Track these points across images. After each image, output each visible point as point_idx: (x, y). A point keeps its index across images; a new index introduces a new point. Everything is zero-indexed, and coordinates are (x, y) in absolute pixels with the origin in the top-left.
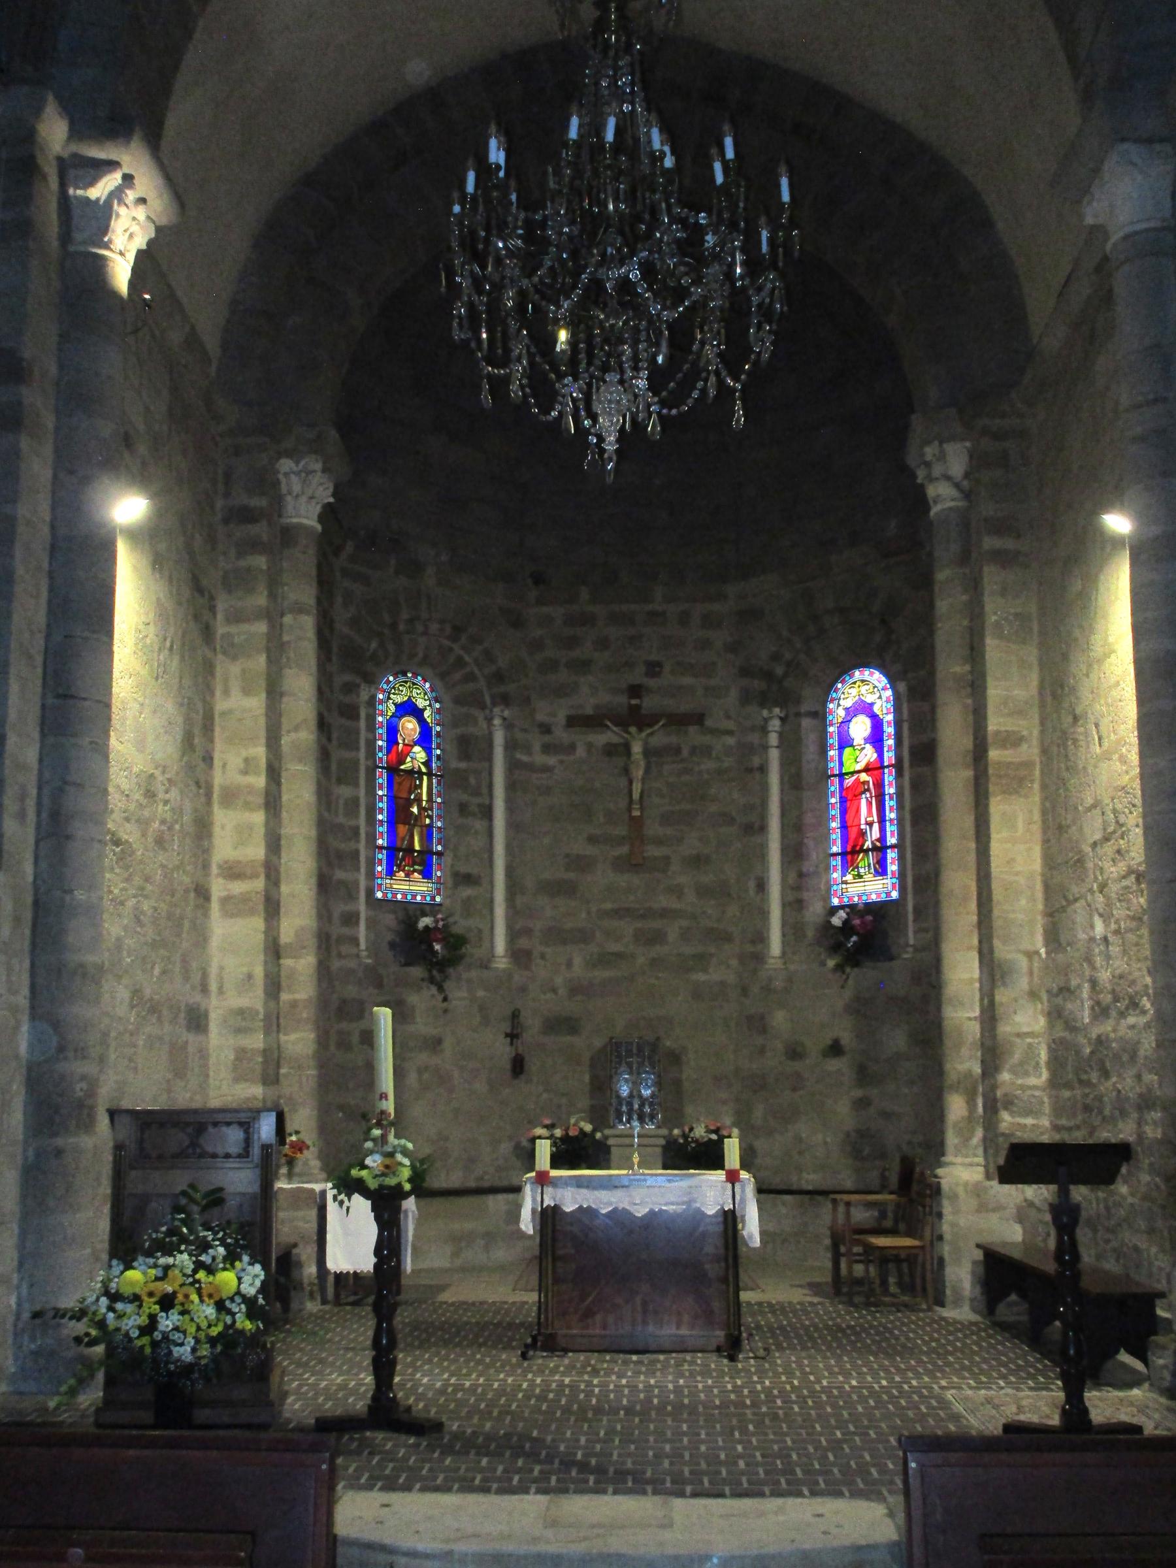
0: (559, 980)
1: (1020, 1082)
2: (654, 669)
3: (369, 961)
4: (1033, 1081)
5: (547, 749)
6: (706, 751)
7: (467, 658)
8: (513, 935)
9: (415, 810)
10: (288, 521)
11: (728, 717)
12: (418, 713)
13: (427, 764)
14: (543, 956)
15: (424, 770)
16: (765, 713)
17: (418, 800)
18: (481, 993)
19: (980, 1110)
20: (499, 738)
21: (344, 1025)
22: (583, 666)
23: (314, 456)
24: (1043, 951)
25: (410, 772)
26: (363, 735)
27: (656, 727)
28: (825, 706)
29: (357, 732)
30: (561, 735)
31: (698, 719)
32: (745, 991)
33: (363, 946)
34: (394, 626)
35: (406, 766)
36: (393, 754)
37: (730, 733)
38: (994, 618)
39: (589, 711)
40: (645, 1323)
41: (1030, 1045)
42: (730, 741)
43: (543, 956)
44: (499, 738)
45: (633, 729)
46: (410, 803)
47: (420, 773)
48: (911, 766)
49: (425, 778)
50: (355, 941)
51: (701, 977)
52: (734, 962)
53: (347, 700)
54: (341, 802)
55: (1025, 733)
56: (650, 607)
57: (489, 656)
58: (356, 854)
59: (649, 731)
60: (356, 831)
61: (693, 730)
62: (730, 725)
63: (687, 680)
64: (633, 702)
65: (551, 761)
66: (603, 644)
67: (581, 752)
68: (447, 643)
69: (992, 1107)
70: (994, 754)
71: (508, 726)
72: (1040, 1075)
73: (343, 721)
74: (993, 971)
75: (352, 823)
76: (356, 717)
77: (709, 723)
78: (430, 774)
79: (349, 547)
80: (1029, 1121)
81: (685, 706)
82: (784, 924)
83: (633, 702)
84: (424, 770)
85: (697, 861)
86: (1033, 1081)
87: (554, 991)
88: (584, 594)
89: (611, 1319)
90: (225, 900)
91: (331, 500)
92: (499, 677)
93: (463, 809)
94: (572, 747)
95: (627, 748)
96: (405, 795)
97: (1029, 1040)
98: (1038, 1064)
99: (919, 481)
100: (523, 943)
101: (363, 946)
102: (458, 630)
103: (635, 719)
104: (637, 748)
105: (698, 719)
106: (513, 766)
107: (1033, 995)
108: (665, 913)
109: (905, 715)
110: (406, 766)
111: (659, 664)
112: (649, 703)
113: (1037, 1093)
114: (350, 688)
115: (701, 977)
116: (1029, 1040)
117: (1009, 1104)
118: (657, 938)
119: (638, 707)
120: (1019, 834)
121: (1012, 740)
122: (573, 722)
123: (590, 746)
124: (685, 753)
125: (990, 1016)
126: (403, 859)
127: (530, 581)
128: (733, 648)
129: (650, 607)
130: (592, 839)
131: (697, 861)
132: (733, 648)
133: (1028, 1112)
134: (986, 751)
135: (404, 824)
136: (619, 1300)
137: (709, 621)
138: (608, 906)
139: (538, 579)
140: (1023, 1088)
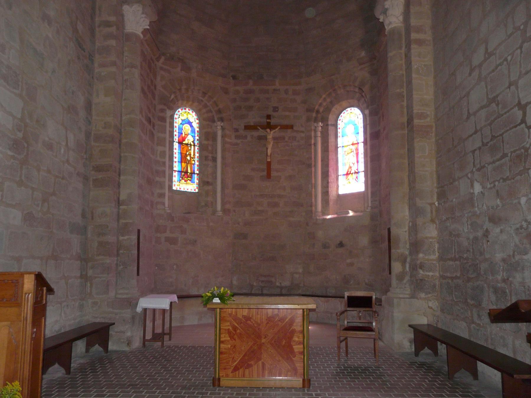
0: (240, 220)
1: (427, 257)
2: (275, 109)
3: (169, 211)
4: (433, 257)
5: (237, 137)
6: (294, 138)
7: (208, 104)
8: (223, 203)
9: (188, 158)
10: (128, 31)
11: (302, 126)
12: (190, 123)
13: (193, 142)
14: (234, 211)
15: (192, 144)
16: (315, 124)
17: (190, 155)
18: (211, 224)
19: (408, 269)
20: (219, 133)
21: (159, 235)
22: (250, 108)
23: (138, 4)
24: (436, 203)
25: (187, 144)
26: (168, 129)
27: (277, 130)
28: (337, 122)
29: (165, 126)
30: (242, 132)
31: (291, 127)
32: (307, 224)
33: (167, 205)
34: (180, 90)
35: (186, 142)
36: (181, 138)
37: (302, 132)
38: (415, 66)
39: (252, 124)
40: (263, 376)
41: (431, 242)
42: (303, 135)
43: (234, 211)
44: (219, 133)
45: (268, 130)
46: (186, 155)
47: (191, 145)
48: (370, 140)
49: (192, 147)
50: (164, 204)
51: (292, 219)
52: (304, 214)
53: (161, 114)
54: (159, 153)
55: (429, 113)
56: (274, 87)
57: (215, 103)
58: (164, 172)
59: (274, 131)
60: (164, 163)
61: (289, 131)
62: (303, 129)
63: (287, 113)
64: (268, 121)
65: (239, 141)
66: (258, 100)
67: (249, 138)
68: (201, 98)
69: (414, 268)
70: (416, 121)
71: (223, 129)
72: (435, 255)
73: (160, 123)
74: (416, 212)
75: (163, 160)
76: (165, 122)
77: (294, 128)
78: (194, 145)
79: (162, 59)
80: (431, 274)
81: (285, 122)
82: (322, 200)
83: (268, 121)
84: (192, 144)
85: (290, 178)
86: (433, 257)
87: (239, 224)
88: (251, 82)
89: (247, 371)
90: (95, 181)
91: (148, 28)
92: (219, 111)
93: (206, 158)
94: (246, 137)
95: (265, 138)
96: (185, 153)
97: (431, 240)
98: (434, 249)
99: (381, 20)
100: (228, 206)
101: (167, 205)
102: (205, 94)
103: (269, 126)
104: (270, 137)
105: (291, 127)
106: (224, 143)
107: (433, 221)
108: (280, 196)
109: (368, 122)
110: (186, 142)
111: (277, 108)
112: (273, 122)
113: (434, 262)
114: (162, 111)
115: (292, 219)
116: (431, 240)
117: (421, 267)
118: (276, 205)
119: (270, 123)
120: (426, 155)
121: (422, 116)
122: (247, 127)
123: (252, 136)
124: (286, 139)
125: (414, 229)
126: (184, 175)
127: (231, 78)
128: (304, 102)
129: (274, 87)
130: (253, 169)
131: (290, 178)
132: (304, 102)
133: (430, 270)
134: (412, 120)
135: (185, 163)
136: (252, 362)
137: (295, 93)
138: (258, 194)
139: (234, 77)
140: (428, 260)
